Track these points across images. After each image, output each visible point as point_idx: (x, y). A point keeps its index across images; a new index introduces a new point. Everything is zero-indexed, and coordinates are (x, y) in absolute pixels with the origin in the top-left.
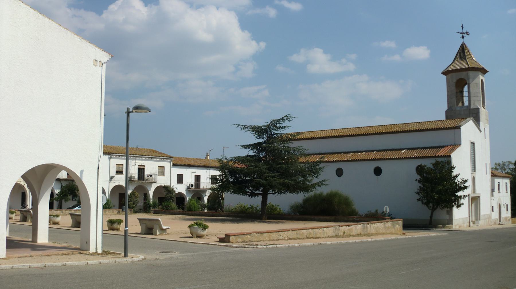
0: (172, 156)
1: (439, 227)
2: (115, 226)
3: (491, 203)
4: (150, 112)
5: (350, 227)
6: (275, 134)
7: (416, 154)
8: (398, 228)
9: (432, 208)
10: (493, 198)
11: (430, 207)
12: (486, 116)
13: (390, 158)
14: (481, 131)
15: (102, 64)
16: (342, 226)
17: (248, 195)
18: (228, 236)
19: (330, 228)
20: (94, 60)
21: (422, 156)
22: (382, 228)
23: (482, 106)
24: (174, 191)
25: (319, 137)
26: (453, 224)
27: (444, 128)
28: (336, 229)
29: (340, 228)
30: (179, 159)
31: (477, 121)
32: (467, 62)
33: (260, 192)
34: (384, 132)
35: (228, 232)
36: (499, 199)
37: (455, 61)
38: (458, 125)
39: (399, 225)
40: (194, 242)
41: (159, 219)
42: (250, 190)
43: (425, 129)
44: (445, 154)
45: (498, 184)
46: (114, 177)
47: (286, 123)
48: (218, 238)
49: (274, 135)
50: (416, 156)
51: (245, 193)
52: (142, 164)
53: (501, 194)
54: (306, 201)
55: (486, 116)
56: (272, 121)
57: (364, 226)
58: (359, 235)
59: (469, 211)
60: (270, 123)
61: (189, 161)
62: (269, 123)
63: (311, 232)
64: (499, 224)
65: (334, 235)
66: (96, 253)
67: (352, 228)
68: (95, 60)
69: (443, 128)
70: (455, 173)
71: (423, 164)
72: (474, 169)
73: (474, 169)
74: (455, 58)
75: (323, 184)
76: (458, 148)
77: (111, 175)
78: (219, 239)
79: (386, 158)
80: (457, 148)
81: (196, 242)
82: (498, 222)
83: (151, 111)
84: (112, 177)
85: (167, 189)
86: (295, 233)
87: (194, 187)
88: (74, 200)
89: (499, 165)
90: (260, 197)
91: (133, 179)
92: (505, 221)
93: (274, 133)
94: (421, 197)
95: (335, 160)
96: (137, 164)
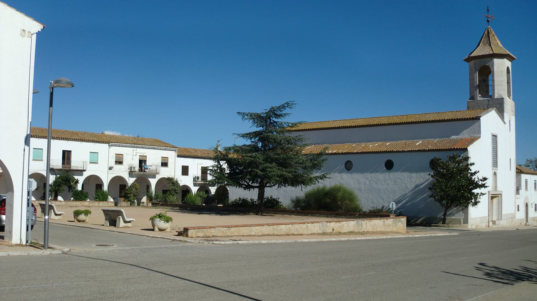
0: (176, 146)
1: (432, 226)
2: (82, 217)
3: (515, 202)
4: (73, 86)
5: (340, 224)
6: (274, 123)
7: (430, 147)
8: (401, 226)
9: (445, 206)
10: (518, 196)
11: (444, 204)
12: (512, 107)
13: (403, 150)
14: (505, 123)
15: (32, 35)
16: (330, 222)
17: (244, 187)
18: (186, 230)
19: (315, 224)
20: (21, 30)
21: (436, 149)
22: (380, 226)
23: (507, 95)
24: (178, 184)
25: (330, 127)
26: (469, 223)
27: (462, 118)
28: (322, 226)
29: (328, 224)
30: (186, 150)
31: (501, 111)
32: (492, 48)
33: (258, 185)
34: (398, 123)
35: (186, 226)
36: (527, 198)
37: (478, 47)
38: (478, 116)
39: (402, 223)
40: (150, 235)
41: (122, 210)
42: (246, 182)
43: (442, 120)
44: (462, 147)
45: (526, 182)
46: (113, 167)
47: (287, 111)
48: (176, 232)
49: (273, 123)
50: (431, 148)
51: (240, 185)
52: (143, 154)
53: (529, 192)
54: (308, 196)
55: (512, 107)
56: (271, 109)
57: (358, 222)
58: (351, 233)
59: (489, 210)
60: (269, 110)
61: (196, 152)
62: (267, 111)
63: (292, 228)
64: (526, 225)
65: (320, 232)
66: (21, 245)
67: (343, 225)
68: (23, 30)
69: (461, 118)
70: (473, 169)
71: (437, 157)
72: (495, 164)
73: (495, 164)
74: (479, 44)
75: (326, 177)
76: (476, 141)
77: (110, 166)
78: (177, 233)
79: (398, 150)
80: (476, 140)
81: (151, 236)
82: (525, 222)
83: (75, 86)
84: (110, 167)
85: (170, 181)
86: (271, 228)
87: (200, 180)
88: (71, 191)
89: (531, 162)
90: (257, 190)
91: (133, 170)
92: (532, 222)
93: (273, 121)
94: (434, 193)
95: (344, 152)
96: (138, 155)
